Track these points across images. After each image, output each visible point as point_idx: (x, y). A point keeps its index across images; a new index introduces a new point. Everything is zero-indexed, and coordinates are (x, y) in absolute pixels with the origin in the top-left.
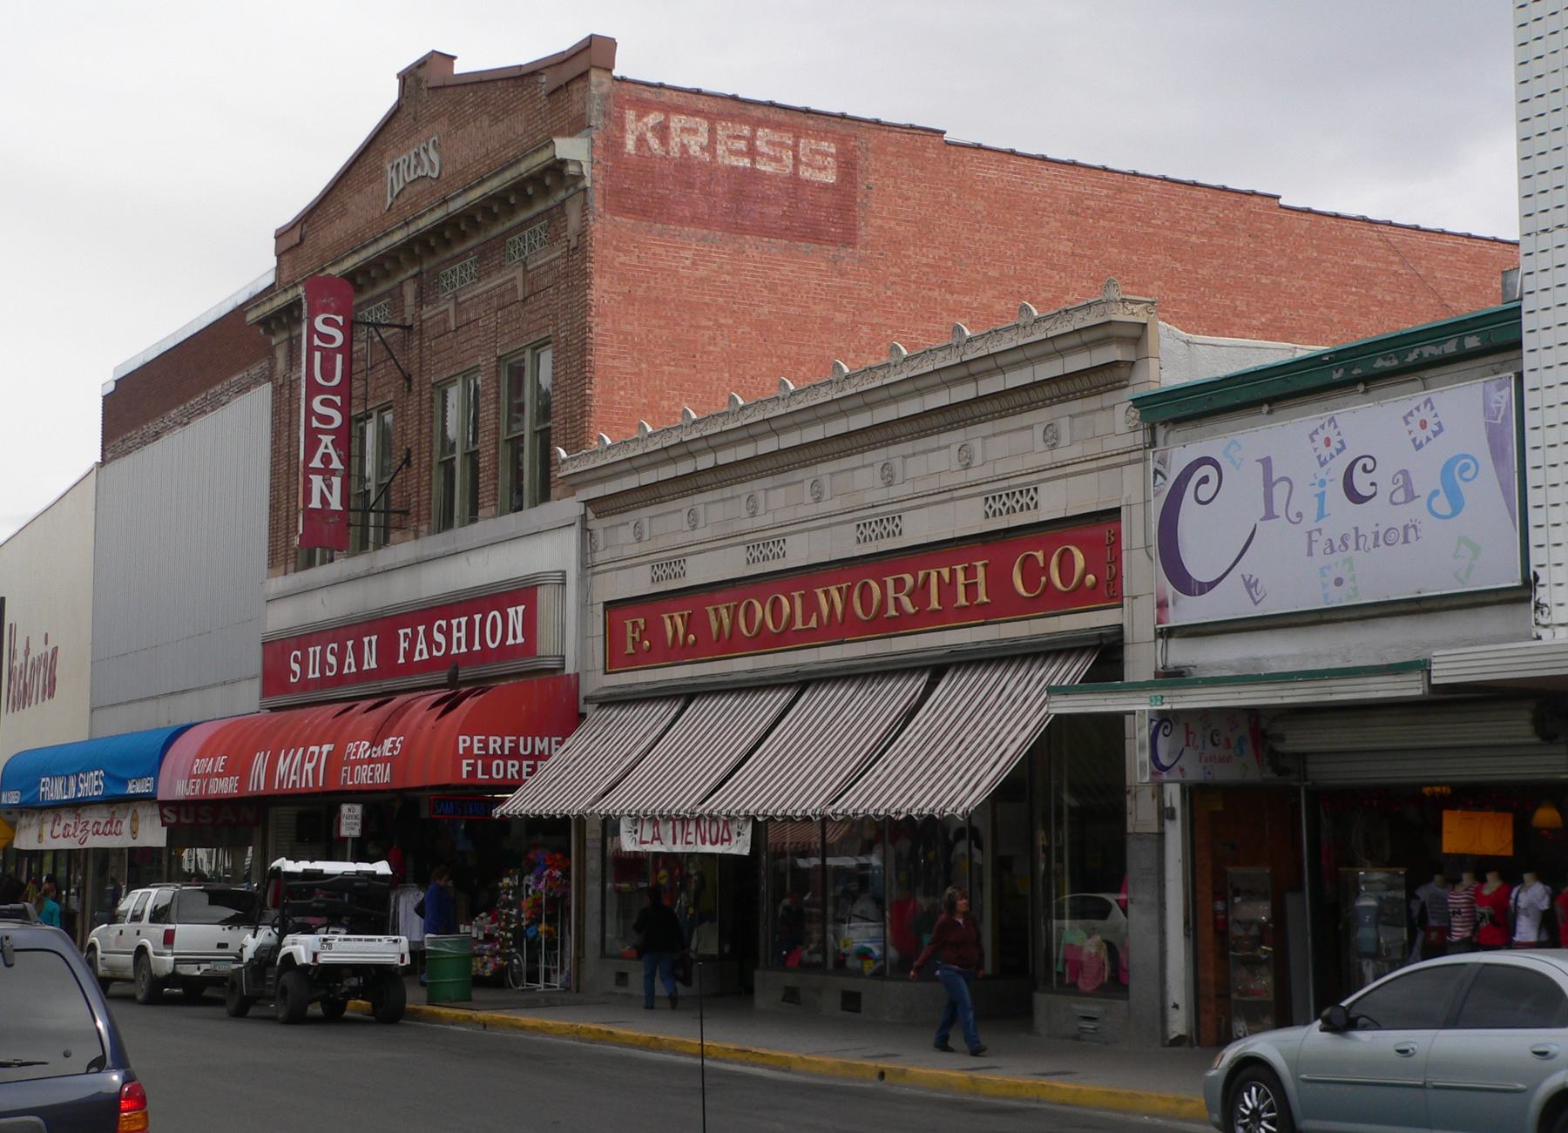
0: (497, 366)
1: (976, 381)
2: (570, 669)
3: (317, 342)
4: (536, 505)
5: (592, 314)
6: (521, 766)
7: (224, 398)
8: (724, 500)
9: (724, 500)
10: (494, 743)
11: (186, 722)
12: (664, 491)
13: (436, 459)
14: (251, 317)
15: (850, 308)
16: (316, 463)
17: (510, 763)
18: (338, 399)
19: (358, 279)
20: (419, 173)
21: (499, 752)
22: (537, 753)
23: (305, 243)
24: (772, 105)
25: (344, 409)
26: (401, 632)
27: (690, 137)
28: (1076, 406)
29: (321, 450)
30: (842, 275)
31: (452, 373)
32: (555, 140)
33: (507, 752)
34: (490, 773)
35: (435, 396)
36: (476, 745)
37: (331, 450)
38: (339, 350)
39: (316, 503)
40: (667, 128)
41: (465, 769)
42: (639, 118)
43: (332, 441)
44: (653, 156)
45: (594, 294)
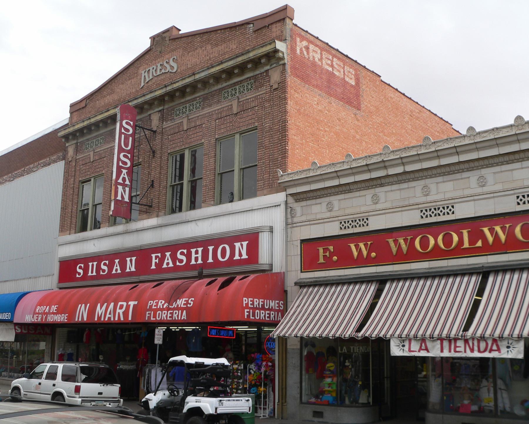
0: (215, 142)
1: (370, 172)
2: (276, 270)
3: (123, 131)
4: (240, 200)
5: (288, 115)
6: (265, 314)
7: (35, 169)
8: (400, 190)
9: (400, 190)
10: (256, 302)
11: (26, 290)
12: (352, 187)
13: (169, 184)
14: (60, 134)
15: (360, 133)
16: (120, 181)
17: (262, 311)
18: (129, 155)
19: (141, 108)
20: (163, 71)
21: (258, 307)
22: (271, 308)
23: (87, 107)
24: (337, 50)
25: (132, 160)
26: (154, 256)
27: (315, 54)
28: (342, 196)
29: (122, 176)
30: (358, 120)
31: (183, 147)
32: (276, 41)
33: (260, 307)
34: (156, 318)
35: (169, 158)
36: (250, 303)
37: (126, 176)
38: (131, 135)
39: (119, 198)
40: (309, 48)
41: (246, 314)
42: (301, 42)
43: (127, 172)
44: (305, 58)
45: (289, 108)
